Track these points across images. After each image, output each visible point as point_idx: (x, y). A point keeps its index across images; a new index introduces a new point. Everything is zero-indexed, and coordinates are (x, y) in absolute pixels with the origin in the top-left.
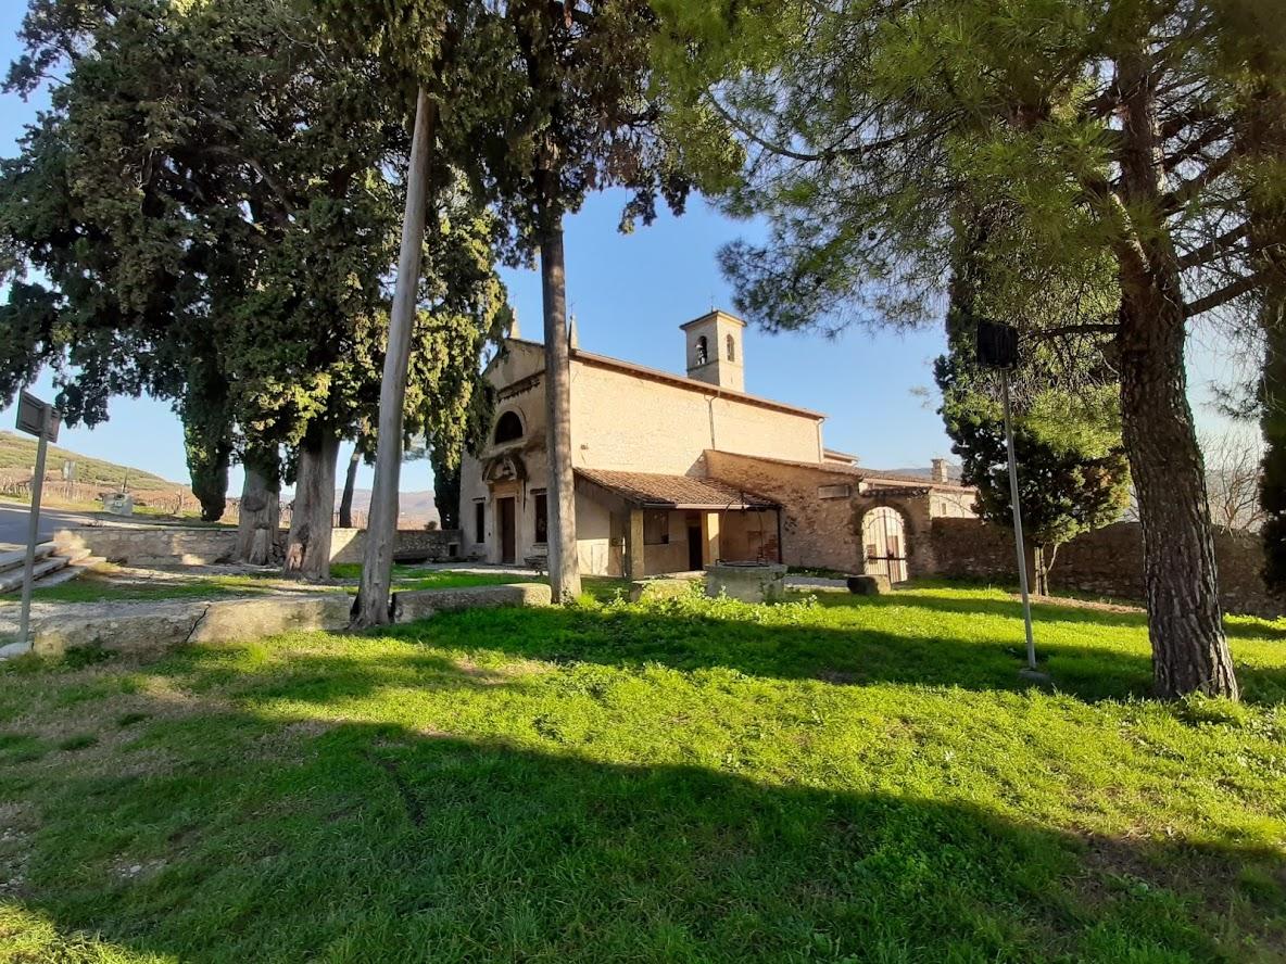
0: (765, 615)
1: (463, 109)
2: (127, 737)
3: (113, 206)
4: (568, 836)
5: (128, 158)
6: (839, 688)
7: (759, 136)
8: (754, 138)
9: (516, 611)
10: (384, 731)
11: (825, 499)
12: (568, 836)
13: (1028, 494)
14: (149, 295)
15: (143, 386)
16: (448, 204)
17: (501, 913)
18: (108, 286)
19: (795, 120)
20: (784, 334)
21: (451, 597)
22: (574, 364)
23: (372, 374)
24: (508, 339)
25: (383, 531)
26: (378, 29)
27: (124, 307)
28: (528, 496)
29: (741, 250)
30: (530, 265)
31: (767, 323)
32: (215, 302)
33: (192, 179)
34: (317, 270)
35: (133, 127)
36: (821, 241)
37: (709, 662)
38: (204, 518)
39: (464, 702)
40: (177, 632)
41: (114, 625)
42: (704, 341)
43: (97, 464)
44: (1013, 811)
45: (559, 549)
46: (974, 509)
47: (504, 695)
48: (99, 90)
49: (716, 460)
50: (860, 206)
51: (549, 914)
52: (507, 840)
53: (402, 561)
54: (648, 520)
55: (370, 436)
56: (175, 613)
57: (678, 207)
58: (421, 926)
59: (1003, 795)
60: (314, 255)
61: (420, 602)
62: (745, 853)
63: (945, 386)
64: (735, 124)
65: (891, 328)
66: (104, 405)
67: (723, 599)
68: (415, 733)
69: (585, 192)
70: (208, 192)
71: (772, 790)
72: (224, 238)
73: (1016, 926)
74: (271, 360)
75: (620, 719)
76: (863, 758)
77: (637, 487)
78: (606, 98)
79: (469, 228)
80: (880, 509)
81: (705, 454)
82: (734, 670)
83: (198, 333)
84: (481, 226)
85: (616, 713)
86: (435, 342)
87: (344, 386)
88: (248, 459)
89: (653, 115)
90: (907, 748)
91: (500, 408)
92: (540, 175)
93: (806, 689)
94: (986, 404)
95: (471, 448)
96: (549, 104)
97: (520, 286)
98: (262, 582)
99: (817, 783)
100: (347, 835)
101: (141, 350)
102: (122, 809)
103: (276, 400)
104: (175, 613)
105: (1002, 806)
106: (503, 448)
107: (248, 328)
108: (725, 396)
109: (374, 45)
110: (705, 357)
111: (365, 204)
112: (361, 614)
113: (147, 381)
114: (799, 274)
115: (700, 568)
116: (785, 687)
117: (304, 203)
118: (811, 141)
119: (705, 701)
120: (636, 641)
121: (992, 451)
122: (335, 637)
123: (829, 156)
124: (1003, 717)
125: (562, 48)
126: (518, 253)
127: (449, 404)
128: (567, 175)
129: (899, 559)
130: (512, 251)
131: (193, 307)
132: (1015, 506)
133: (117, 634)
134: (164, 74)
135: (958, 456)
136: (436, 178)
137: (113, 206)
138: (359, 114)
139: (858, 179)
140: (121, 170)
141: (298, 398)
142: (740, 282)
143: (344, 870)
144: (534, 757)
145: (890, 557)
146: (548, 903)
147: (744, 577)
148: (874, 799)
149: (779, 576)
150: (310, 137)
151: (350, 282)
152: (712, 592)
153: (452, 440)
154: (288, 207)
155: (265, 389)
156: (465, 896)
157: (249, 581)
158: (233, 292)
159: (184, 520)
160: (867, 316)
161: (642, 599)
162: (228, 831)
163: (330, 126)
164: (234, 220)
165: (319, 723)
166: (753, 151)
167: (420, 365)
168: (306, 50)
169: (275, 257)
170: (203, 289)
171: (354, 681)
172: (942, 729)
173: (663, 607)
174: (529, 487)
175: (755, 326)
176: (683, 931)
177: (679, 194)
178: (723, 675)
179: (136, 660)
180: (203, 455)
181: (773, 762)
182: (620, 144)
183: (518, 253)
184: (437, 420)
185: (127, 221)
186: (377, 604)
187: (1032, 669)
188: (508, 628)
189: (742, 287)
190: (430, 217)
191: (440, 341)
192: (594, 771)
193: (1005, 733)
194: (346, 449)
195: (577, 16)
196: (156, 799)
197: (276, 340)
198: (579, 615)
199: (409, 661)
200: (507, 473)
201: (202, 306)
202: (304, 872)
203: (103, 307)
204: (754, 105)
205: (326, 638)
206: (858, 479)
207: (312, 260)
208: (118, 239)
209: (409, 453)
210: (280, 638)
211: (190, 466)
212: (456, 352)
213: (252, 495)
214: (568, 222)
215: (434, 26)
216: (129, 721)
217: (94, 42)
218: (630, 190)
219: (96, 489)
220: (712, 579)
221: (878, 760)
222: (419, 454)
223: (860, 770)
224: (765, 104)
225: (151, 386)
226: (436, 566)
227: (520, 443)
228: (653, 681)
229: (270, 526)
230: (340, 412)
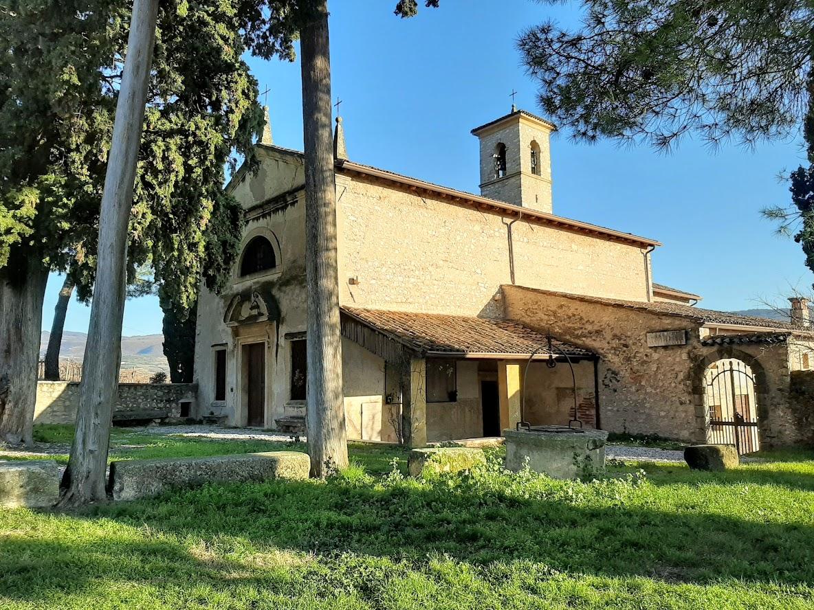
0: (580, 494)
6: (675, 587)
20: (605, 143)
22: (341, 179)
23: (89, 189)
28: (282, 341)
29: (550, 36)
30: (286, 55)
31: (582, 127)
34: (28, 62)
37: (510, 552)
42: (502, 149)
45: (321, 408)
49: (514, 296)
53: (122, 422)
55: (85, 265)
65: (737, 135)
67: (525, 474)
77: (417, 329)
79: (212, 9)
80: (727, 361)
81: (502, 290)
82: (541, 565)
86: (168, 149)
87: (55, 204)
91: (248, 231)
93: (632, 588)
97: (275, 81)
106: (251, 282)
108: (529, 218)
114: (623, 65)
116: (606, 586)
120: (417, 526)
122: (41, 517)
126: (271, 40)
129: (750, 424)
142: (548, 76)
145: (738, 421)
147: (552, 446)
151: (66, 77)
152: (513, 463)
153: (187, 271)
160: (708, 119)
161: (425, 472)
167: (149, 178)
173: (451, 483)
174: (284, 330)
175: (567, 131)
178: (527, 570)
183: (271, 40)
184: (169, 247)
186: (92, 477)
188: (256, 508)
189: (550, 83)
191: (174, 148)
194: (56, 281)
198: (345, 492)
199: (132, 548)
200: (255, 312)
205: (30, 517)
206: (698, 322)
207: (20, 51)
220: (512, 447)
222: (145, 289)
226: (163, 430)
227: (272, 276)
228: (439, 577)
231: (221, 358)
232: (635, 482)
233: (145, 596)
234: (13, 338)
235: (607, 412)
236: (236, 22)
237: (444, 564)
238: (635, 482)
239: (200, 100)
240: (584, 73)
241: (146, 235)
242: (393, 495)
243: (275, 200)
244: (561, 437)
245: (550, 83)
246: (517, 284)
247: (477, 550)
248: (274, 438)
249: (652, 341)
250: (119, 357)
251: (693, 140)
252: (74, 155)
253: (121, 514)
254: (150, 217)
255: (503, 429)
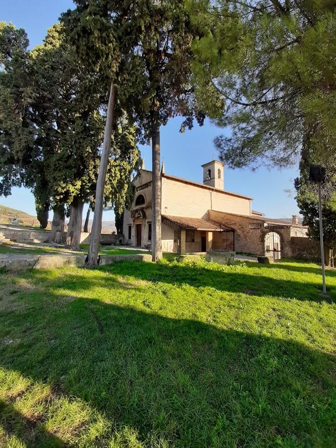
0: (226, 269)
1: (125, 89)
2: (12, 298)
3: (12, 124)
4: (150, 341)
5: (17, 108)
6: (251, 297)
7: (229, 97)
8: (228, 98)
9: (140, 263)
10: (93, 301)
11: (251, 229)
12: (150, 341)
13: (328, 229)
14: (24, 154)
15: (22, 184)
16: (121, 122)
17: (126, 365)
18: (12, 150)
19: (244, 91)
20: (237, 169)
21: (118, 257)
22: (163, 179)
23: (95, 181)
24: (141, 169)
25: (96, 234)
26: (98, 62)
27: (16, 158)
28: (146, 224)
29: (223, 138)
30: (148, 144)
31: (231, 165)
32: (45, 156)
33: (38, 115)
34: (77, 145)
35: (18, 97)
36: (252, 135)
37: (205, 285)
38: (41, 227)
39: (120, 293)
40: (30, 265)
41: (10, 262)
42: (210, 171)
43: (8, 209)
44: (311, 345)
45: (155, 243)
46: (307, 234)
47: (133, 292)
48: (7, 84)
49: (212, 214)
50: (265, 122)
51: (142, 367)
52: (131, 341)
53: (103, 244)
54: (187, 234)
55: (94, 202)
56: (29, 258)
57: (201, 123)
58: (99, 367)
59: (308, 339)
60: (76, 141)
61: (108, 259)
62: (212, 352)
63: (297, 188)
64: (221, 93)
65: (277, 167)
66: (10, 189)
67: (211, 262)
68: (103, 302)
69: (168, 118)
70: (42, 119)
71: (223, 331)
72: (47, 134)
73: (308, 386)
74: (62, 176)
75: (172, 302)
76: (257, 322)
77: (184, 222)
78: (176, 85)
79: (128, 131)
80: (272, 233)
81: (208, 211)
82: (213, 288)
83: (39, 166)
84: (132, 130)
85: (171, 300)
86: (116, 170)
87: (85, 185)
88: (54, 208)
89: (193, 90)
90: (274, 320)
91: (137, 194)
92: (152, 112)
93: (239, 296)
94: (313, 196)
95: (127, 207)
96: (156, 87)
97: (145, 151)
98: (58, 249)
99: (240, 330)
100: (78, 335)
101: (22, 172)
102: (8, 322)
103: (63, 189)
104: (29, 258)
105: (307, 343)
106: (138, 207)
107: (55, 165)
108: (216, 191)
109: (97, 68)
110: (210, 176)
111: (93, 122)
112: (88, 262)
113: (23, 182)
114: (243, 148)
115: (205, 251)
116: (231, 295)
117: (74, 122)
118: (248, 97)
119: (202, 298)
120: (180, 276)
121: (314, 212)
122: (80, 269)
123: (255, 104)
124: (311, 311)
125: (161, 67)
126: (144, 140)
127: (120, 192)
128: (162, 112)
129: (278, 251)
130: (142, 139)
131: (38, 158)
132: (322, 235)
133: (11, 264)
134: (28, 78)
135: (302, 215)
136: (117, 114)
137: (12, 124)
138: (92, 92)
139: (267, 112)
140: (15, 112)
141: (70, 189)
142: (221, 150)
143: (76, 346)
144: (142, 313)
145: (275, 250)
146: (142, 363)
147: (219, 255)
148: (260, 337)
149: (232, 255)
150: (76, 100)
151: (88, 150)
152: (208, 260)
153: (121, 204)
154: (68, 124)
155: (60, 185)
156: (115, 359)
157: (54, 249)
158: (51, 153)
159: (35, 228)
160: (267, 163)
161: (184, 261)
162: (41, 331)
163: (82, 96)
164: (51, 129)
165: (72, 297)
166: (228, 102)
167: (110, 178)
168: (75, 70)
169: (64, 141)
170: (41, 152)
171: (84, 284)
172: (288, 314)
173: (190, 264)
174: (147, 221)
175: (227, 166)
176: (187, 377)
177: (202, 118)
178: (209, 289)
179: (17, 273)
180: (40, 207)
181: (225, 321)
182: (181, 101)
183: (144, 140)
184: (116, 197)
185: (17, 128)
186: (94, 259)
187: (324, 294)
188: (136, 269)
189: (222, 152)
190: (114, 127)
191: (117, 170)
192: (162, 320)
193: (311, 317)
194: (86, 206)
195: (167, 55)
196: (18, 319)
197: (63, 169)
198: (161, 266)
199: (103, 278)
200: (139, 215)
201: (41, 158)
202: (64, 345)
203: (10, 157)
204: (229, 85)
205: (77, 269)
206: (264, 222)
207: (75, 142)
208: (14, 135)
209: (107, 208)
210: (62, 268)
211: (36, 210)
212: (122, 174)
213: (55, 220)
214: (162, 129)
215: (117, 60)
216: (13, 293)
217: (5, 67)
218: (184, 117)
219: (8, 217)
220: (209, 255)
221: (262, 323)
222: (110, 208)
223: (256, 326)
224: (232, 86)
225: (25, 184)
226: (115, 246)
227: (144, 206)
228: (185, 290)
229: (61, 231)
230: (84, 194)
231: (130, 228)
232: (242, 266)
233: (106, 292)
234: (74, 221)
235: (236, 246)
236: (135, 134)
237: (186, 286)
238: (242, 266)
239: (125, 156)
240: (232, 150)
241: (110, 194)
242: (174, 267)
243: (145, 184)
244: (222, 253)
245: (222, 152)
246: (213, 209)
247: (196, 283)
248: (144, 250)
249: (250, 227)
250: (101, 227)
251: (263, 169)
252: (90, 172)
253: (101, 269)
254: (111, 189)
255: (207, 250)
